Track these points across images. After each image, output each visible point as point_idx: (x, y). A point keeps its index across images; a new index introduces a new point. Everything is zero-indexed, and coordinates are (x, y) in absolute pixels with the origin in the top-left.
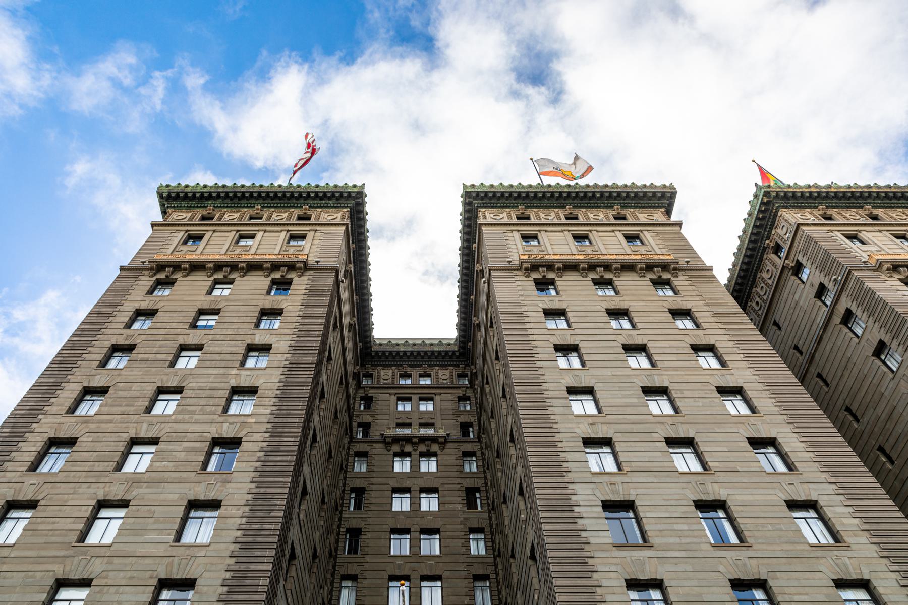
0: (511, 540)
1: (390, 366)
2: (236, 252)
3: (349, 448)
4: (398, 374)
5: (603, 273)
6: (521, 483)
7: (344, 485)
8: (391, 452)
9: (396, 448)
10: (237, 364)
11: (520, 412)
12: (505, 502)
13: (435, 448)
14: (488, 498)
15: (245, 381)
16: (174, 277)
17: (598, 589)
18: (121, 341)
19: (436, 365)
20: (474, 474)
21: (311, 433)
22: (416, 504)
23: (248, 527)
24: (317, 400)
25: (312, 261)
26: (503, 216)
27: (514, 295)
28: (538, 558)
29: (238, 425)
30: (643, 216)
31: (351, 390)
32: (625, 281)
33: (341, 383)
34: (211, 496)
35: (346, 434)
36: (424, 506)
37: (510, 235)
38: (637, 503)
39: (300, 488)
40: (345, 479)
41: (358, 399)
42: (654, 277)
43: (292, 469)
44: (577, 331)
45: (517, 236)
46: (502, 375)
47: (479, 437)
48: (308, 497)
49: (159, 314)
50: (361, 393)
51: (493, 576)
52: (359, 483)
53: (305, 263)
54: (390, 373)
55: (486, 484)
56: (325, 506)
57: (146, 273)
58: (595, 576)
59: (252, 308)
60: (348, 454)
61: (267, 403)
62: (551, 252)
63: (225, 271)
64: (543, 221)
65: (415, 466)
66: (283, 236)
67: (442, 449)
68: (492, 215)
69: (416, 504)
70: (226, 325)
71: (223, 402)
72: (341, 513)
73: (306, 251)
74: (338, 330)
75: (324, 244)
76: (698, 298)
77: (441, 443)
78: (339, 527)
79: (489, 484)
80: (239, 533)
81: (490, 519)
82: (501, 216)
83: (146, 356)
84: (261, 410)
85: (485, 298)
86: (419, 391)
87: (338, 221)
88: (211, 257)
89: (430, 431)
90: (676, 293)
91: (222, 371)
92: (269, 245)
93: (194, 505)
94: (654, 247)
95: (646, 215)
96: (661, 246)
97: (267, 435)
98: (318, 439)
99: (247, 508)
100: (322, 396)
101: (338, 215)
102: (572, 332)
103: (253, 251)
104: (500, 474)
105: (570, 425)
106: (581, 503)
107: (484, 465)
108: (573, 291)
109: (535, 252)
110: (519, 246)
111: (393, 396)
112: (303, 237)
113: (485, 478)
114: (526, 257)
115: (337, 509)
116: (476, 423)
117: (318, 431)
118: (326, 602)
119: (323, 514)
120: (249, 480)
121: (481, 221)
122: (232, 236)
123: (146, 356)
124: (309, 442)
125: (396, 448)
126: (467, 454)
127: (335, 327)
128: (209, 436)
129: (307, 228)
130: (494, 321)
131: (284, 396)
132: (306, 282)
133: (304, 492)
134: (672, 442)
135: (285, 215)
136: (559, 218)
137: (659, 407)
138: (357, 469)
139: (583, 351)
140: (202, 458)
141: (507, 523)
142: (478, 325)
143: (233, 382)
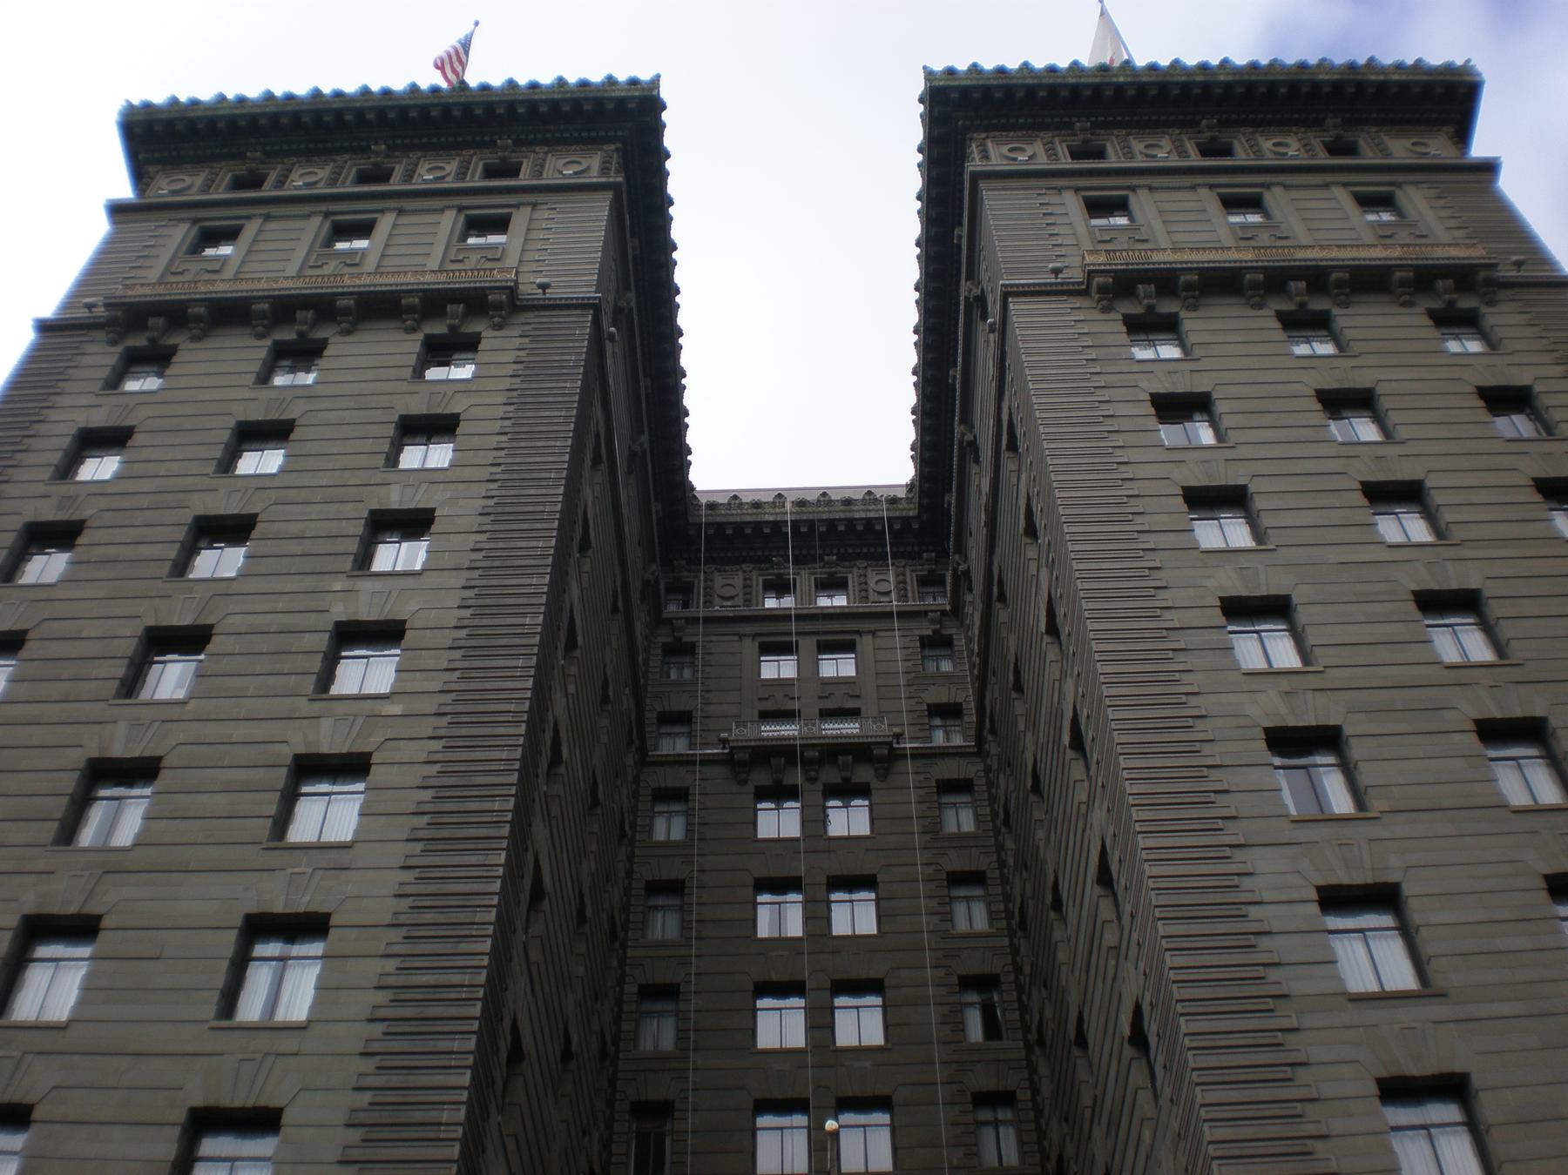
0: (1074, 999)
1: (739, 561)
2: (327, 270)
3: (637, 780)
4: (758, 581)
5: (1305, 296)
6: (1103, 854)
7: (629, 874)
8: (750, 788)
9: (761, 778)
10: (347, 563)
11: (1100, 668)
12: (1057, 904)
13: (864, 774)
14: (1008, 898)
15: (366, 606)
16: (171, 341)
17: (1309, 1107)
18: (48, 512)
19: (859, 556)
20: (967, 836)
21: (548, 736)
22: (817, 917)
23: (401, 980)
24: (560, 652)
25: (527, 289)
26: (1033, 153)
27: (1063, 360)
28: (1153, 1040)
29: (360, 721)
30: (1400, 149)
31: (639, 629)
32: (1362, 320)
33: (615, 610)
34: (304, 902)
35: (630, 742)
36: (841, 924)
37: (1055, 199)
38: (1407, 889)
39: (527, 883)
40: (631, 857)
41: (657, 651)
42: (1437, 304)
43: (506, 831)
44: (1244, 452)
45: (1072, 204)
46: (1044, 573)
47: (980, 740)
48: (546, 904)
49: (138, 439)
50: (663, 637)
51: (1024, 1095)
52: (669, 870)
53: (512, 291)
54: (738, 580)
55: (1002, 864)
56: (587, 929)
57: (100, 335)
58: (1302, 1075)
59: (377, 415)
60: (636, 795)
61: (431, 664)
62: (1164, 242)
63: (298, 326)
64: (1140, 162)
65: (814, 822)
66: (449, 221)
67: (884, 775)
68: (1005, 149)
69: (817, 917)
70: (312, 463)
71: (316, 664)
72: (624, 947)
73: (512, 261)
74: (604, 467)
75: (556, 247)
76: (1548, 358)
77: (881, 759)
78: (621, 982)
79: (1011, 861)
80: (382, 997)
81: (1015, 951)
82: (1030, 151)
83: (111, 550)
84: (418, 683)
85: (991, 369)
86: (819, 626)
87: (594, 177)
88: (263, 285)
89: (850, 728)
90: (1492, 344)
91: (308, 583)
92: (412, 247)
93: (260, 927)
94: (1431, 229)
95: (1408, 143)
96: (1452, 223)
97: (437, 745)
98: (565, 755)
99: (396, 935)
100: (571, 644)
101: (591, 165)
102: (1229, 454)
103: (370, 264)
104: (1041, 834)
105: (1231, 698)
106: (1266, 896)
107: (994, 815)
108: (1228, 347)
109: (1122, 242)
110: (1081, 228)
111: (747, 642)
112: (500, 224)
113: (1000, 847)
114: (1102, 259)
115: (613, 936)
116: (970, 706)
117: (563, 734)
118: (597, 1168)
119: (582, 949)
120: (398, 860)
121: (975, 164)
122: (314, 227)
123: (111, 550)
124: (544, 762)
125: (761, 778)
126: (949, 787)
127: (597, 461)
128: (286, 753)
129: (512, 200)
130: (1019, 431)
131: (476, 643)
132: (517, 342)
133: (538, 893)
134: (1494, 732)
135: (451, 167)
136: (1182, 153)
137: (1461, 643)
138: (660, 834)
139: (1437, 498)
140: (272, 809)
141: (1062, 956)
142: (974, 446)
143: (341, 611)
